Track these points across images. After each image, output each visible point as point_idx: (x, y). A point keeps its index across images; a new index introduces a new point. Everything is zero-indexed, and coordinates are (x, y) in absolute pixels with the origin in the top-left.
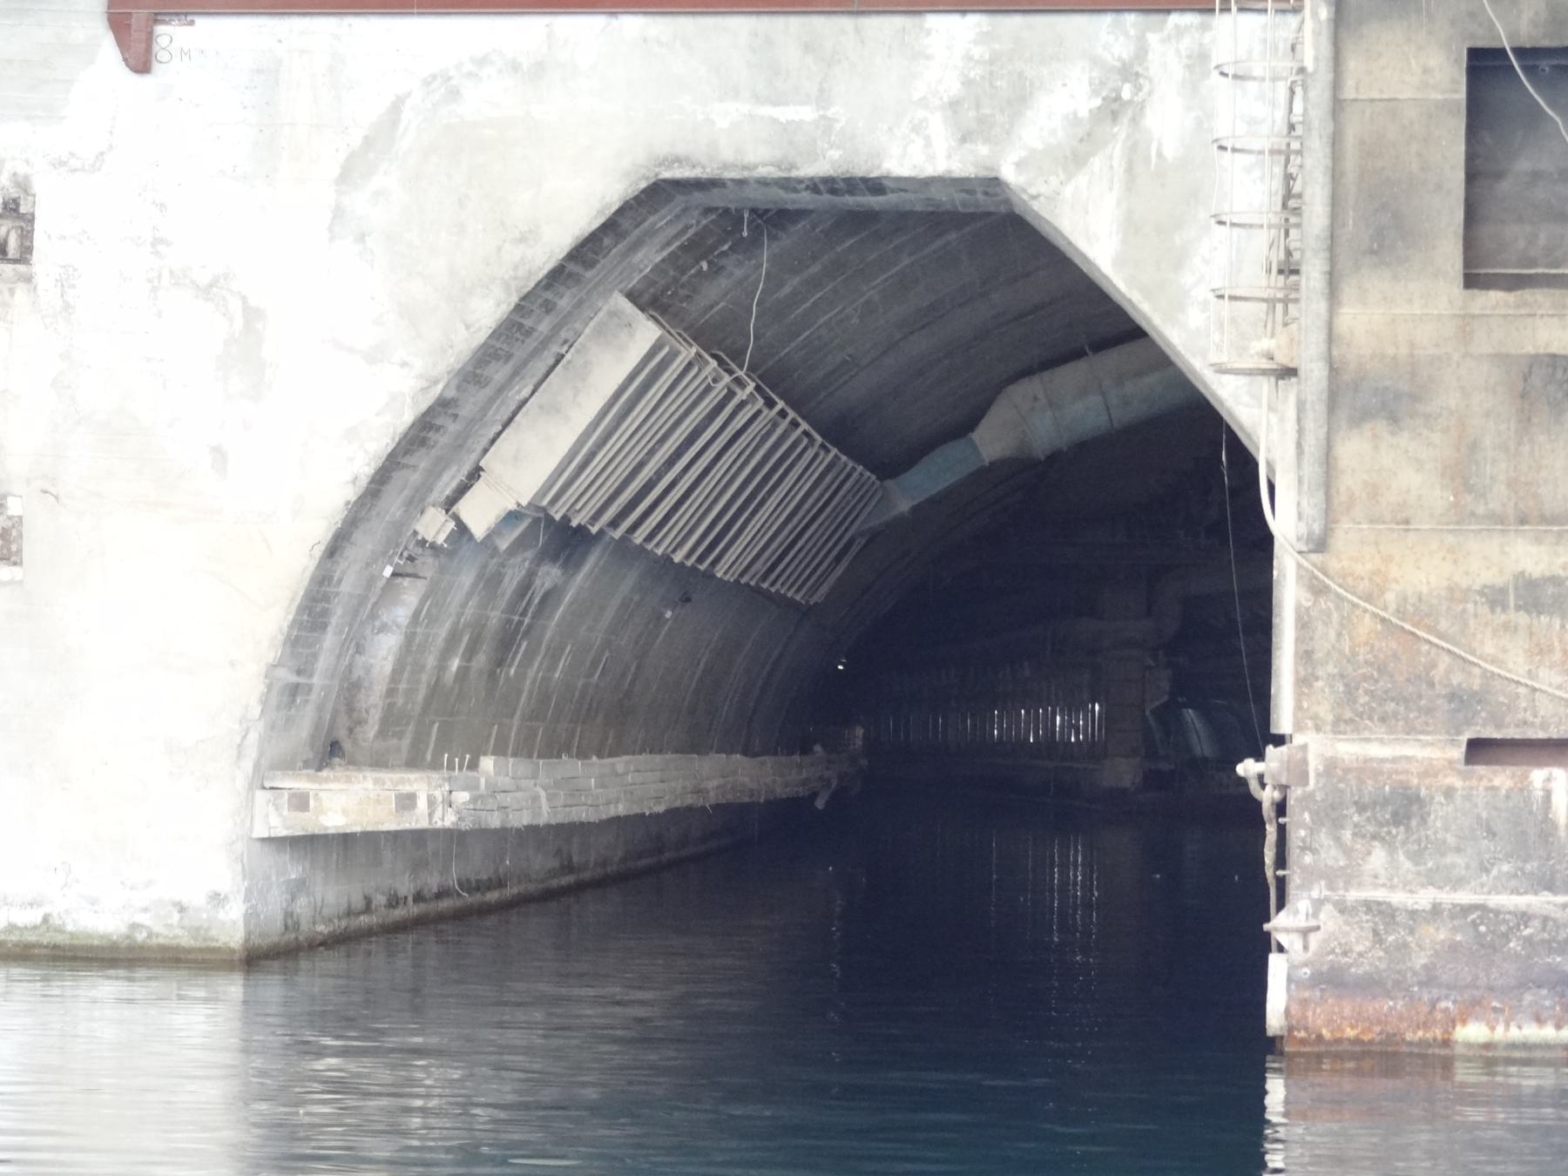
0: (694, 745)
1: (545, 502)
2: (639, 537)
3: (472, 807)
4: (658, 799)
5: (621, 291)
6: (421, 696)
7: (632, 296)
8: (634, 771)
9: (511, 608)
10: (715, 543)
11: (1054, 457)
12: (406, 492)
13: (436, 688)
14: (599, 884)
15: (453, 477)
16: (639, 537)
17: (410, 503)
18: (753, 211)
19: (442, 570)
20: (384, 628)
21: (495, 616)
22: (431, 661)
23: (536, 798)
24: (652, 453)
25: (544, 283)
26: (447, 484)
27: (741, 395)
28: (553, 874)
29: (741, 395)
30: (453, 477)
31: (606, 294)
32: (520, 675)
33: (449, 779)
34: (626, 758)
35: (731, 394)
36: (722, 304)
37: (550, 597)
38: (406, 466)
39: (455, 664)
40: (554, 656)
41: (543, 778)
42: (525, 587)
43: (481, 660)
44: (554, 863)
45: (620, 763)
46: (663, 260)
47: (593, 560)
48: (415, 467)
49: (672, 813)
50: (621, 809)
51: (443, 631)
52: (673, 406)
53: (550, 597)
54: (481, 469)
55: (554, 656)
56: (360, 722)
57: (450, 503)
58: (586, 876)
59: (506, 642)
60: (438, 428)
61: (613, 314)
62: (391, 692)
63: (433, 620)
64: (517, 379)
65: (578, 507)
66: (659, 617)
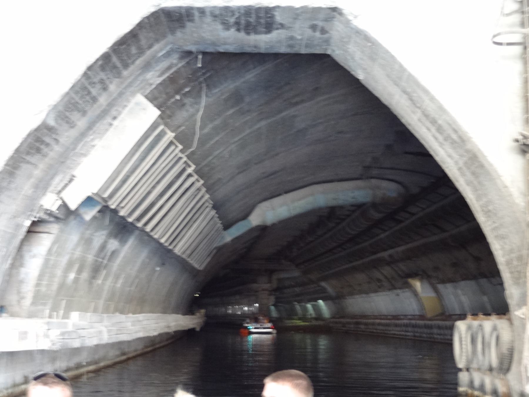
0: (165, 311)
1: (106, 195)
2: (148, 228)
3: (61, 337)
4: (155, 330)
5: (142, 94)
6: (55, 287)
7: (147, 97)
8: (90, 102)
9: (97, 255)
10: (175, 238)
11: (274, 225)
12: (32, 180)
13: (62, 285)
14: (134, 357)
15: (61, 181)
16: (148, 228)
17: (36, 187)
18: (204, 53)
19: (62, 231)
20: (34, 256)
21: (90, 258)
22: (59, 272)
23: (100, 332)
24: (154, 187)
25: (100, 63)
26: (58, 184)
27: (190, 170)
28: (118, 356)
29: (190, 170)
30: (61, 181)
31: (133, 94)
32: (103, 284)
33: (48, 323)
34: (143, 314)
35: (184, 170)
36: (183, 128)
37: (114, 253)
38: (28, 162)
39: (72, 276)
40: (117, 277)
41: (106, 323)
42: (103, 247)
43: (85, 275)
44: (118, 353)
45: (141, 317)
46: (161, 84)
47: (131, 241)
48: (35, 166)
49: (160, 335)
50: (141, 335)
51: (64, 260)
52: (163, 164)
53: (114, 253)
54: (74, 176)
55: (117, 277)
56: (23, 298)
57: (60, 192)
58: (131, 355)
59: (96, 270)
60: (47, 145)
61: (137, 104)
62: (38, 285)
63: (59, 254)
64: (91, 132)
65: (122, 205)
66: (154, 271)
